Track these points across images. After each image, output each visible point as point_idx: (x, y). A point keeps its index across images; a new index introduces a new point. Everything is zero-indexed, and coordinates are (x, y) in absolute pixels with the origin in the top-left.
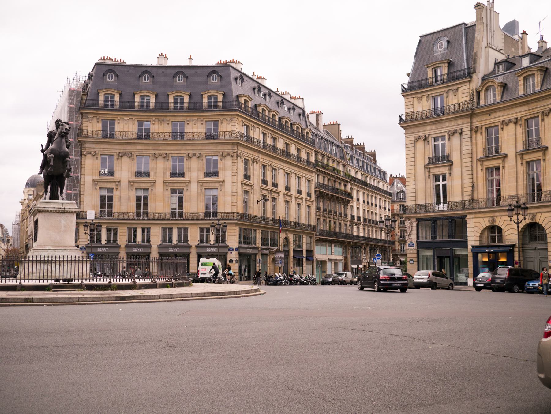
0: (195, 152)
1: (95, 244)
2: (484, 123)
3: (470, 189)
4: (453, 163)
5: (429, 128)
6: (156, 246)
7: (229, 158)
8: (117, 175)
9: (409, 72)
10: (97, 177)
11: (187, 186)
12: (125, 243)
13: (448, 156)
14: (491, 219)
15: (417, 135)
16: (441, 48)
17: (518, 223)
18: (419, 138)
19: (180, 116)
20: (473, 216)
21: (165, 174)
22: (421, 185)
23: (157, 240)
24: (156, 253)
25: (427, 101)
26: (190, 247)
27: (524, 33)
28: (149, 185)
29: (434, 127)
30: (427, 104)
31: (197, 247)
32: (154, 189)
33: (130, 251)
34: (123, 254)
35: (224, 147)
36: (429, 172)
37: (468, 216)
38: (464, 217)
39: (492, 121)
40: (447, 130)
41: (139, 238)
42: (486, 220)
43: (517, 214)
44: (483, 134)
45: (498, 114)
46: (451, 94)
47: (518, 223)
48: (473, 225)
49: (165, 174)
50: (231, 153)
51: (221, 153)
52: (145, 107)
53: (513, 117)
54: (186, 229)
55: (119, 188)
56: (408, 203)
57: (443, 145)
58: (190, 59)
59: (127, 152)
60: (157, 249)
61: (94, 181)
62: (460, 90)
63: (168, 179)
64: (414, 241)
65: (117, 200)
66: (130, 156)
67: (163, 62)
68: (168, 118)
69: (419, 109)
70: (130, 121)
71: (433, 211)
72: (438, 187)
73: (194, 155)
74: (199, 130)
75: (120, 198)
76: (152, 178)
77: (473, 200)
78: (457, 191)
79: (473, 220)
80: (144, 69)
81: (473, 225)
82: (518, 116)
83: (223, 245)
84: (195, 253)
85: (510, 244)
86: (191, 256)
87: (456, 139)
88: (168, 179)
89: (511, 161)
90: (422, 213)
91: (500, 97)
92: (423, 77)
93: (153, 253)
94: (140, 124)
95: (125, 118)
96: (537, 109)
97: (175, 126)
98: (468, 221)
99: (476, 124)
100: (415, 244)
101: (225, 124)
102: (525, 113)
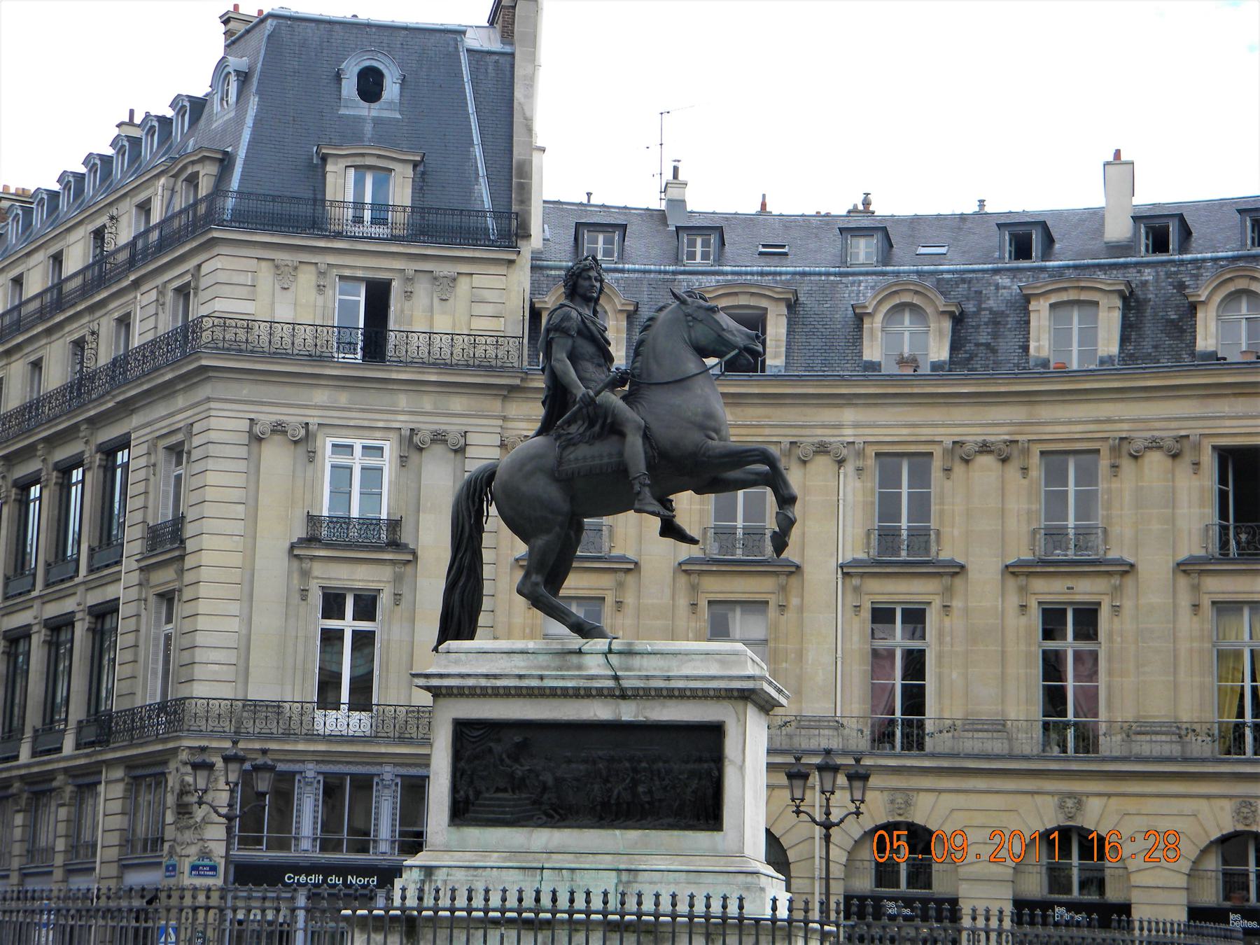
4: (414, 553)
5: (321, 396)
15: (267, 417)
17: (827, 826)
18: (279, 429)
22: (267, 621)
25: (320, 288)
29: (343, 398)
36: (305, 574)
47: (827, 826)
53: (998, 436)
56: (199, 690)
62: (463, 284)
69: (284, 313)
72: (331, 639)
89: (984, 586)
90: (270, 737)
96: (767, 431)
102: (905, 431)
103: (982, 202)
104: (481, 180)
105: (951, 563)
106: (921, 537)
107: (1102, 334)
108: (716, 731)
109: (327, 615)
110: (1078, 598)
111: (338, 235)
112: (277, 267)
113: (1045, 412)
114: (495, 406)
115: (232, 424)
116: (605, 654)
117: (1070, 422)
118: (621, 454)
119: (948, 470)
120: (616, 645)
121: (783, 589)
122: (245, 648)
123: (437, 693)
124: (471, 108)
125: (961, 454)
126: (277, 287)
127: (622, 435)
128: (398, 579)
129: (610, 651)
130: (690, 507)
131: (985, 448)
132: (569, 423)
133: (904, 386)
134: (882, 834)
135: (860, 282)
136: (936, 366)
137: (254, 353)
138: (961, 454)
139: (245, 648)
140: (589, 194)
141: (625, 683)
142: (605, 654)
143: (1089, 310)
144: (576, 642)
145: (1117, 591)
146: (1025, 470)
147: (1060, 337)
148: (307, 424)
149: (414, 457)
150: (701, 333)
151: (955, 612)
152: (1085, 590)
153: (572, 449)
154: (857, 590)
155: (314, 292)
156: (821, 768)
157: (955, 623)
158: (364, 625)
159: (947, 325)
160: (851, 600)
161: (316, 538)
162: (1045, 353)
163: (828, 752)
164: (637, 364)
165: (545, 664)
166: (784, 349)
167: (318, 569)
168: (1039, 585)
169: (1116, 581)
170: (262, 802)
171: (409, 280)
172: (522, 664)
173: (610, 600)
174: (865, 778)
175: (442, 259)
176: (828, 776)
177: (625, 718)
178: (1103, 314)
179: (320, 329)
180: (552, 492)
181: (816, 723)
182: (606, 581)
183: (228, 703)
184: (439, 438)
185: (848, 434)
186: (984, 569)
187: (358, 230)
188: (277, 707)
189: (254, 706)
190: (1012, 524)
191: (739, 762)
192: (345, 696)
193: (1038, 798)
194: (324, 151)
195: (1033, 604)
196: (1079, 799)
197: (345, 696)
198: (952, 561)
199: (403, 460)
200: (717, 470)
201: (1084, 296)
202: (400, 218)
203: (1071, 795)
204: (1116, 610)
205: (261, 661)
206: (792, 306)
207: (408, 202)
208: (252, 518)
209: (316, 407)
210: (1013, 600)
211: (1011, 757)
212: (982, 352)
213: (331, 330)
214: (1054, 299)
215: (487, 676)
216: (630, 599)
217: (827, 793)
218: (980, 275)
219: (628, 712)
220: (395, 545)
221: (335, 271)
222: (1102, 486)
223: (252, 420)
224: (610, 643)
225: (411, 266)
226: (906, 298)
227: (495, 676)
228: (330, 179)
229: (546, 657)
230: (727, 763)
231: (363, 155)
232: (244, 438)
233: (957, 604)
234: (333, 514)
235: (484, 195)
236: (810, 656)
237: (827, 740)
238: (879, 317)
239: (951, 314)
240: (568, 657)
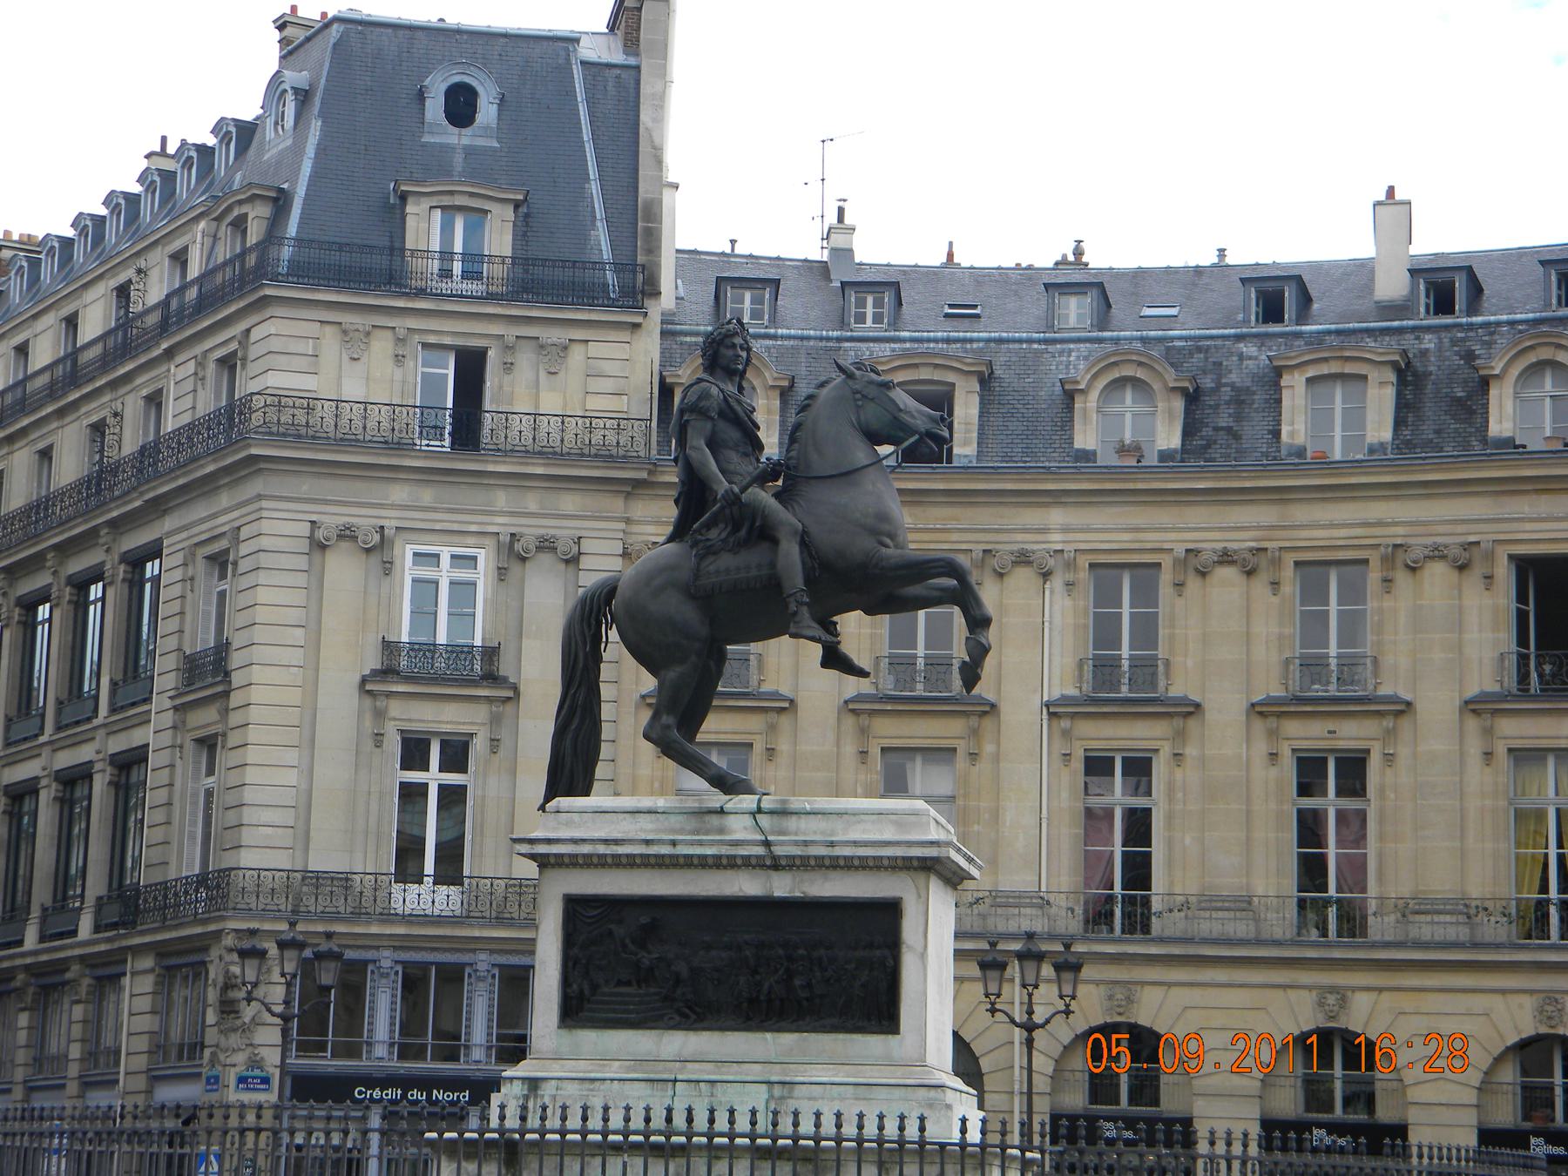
4: (515, 688)
5: (399, 493)
9: (963, 259)
15: (332, 519)
17: (1030, 1027)
22: (333, 772)
25: (399, 359)
29: (427, 495)
36: (380, 715)
42: (1306, 1000)
46: (525, 360)
47: (1030, 1027)
53: (1242, 542)
56: (248, 859)
62: (577, 355)
69: (353, 389)
72: (412, 795)
82: (1484, 535)
90: (336, 917)
96: (955, 537)
103: (1222, 252)
104: (599, 224)
105: (1183, 701)
106: (1146, 668)
107: (1371, 416)
108: (891, 910)
110: (1341, 744)
111: (421, 293)
112: (345, 332)
113: (1301, 513)
114: (616, 505)
116: (753, 814)
117: (1332, 526)
118: (773, 565)
119: (1179, 586)
120: (767, 803)
121: (975, 733)
122: (305, 807)
123: (544, 862)
124: (586, 134)
125: (1196, 565)
126: (345, 357)
127: (775, 542)
128: (495, 721)
129: (759, 810)
130: (859, 631)
131: (1226, 558)
132: (708, 526)
133: (1126, 480)
134: (1097, 1039)
135: (1070, 351)
136: (1165, 456)
137: (315, 439)
138: (1196, 565)
139: (305, 807)
140: (733, 242)
141: (778, 851)
142: (753, 814)
144: (717, 799)
147: (1320, 420)
148: (382, 527)
149: (516, 568)
150: (873, 415)
152: (1350, 734)
153: (711, 558)
154: (1066, 734)
155: (390, 363)
156: (1022, 956)
157: (1189, 775)
158: (453, 778)
159: (1179, 404)
160: (1060, 747)
161: (394, 670)
162: (1300, 440)
164: (793, 453)
165: (678, 826)
166: (975, 435)
167: (396, 708)
168: (1293, 728)
169: (1388, 722)
171: (509, 349)
172: (650, 826)
173: (758, 747)
174: (1076, 968)
176: (1030, 966)
177: (778, 893)
179: (398, 409)
180: (687, 613)
181: (1016, 900)
182: (755, 723)
183: (284, 874)
184: (546, 545)
185: (1056, 540)
187: (445, 287)
189: (317, 879)
191: (920, 949)
193: (1291, 993)
194: (403, 188)
195: (1286, 751)
196: (1343, 995)
197: (429, 866)
198: (1185, 698)
199: (502, 573)
200: (892, 585)
201: (1349, 369)
202: (498, 271)
203: (1333, 989)
204: (1389, 758)
206: (986, 381)
207: (507, 251)
208: (314, 645)
209: (393, 506)
210: (1261, 747)
211: (1259, 942)
212: (1222, 437)
213: (411, 411)
215: (606, 841)
216: (784, 746)
217: (1029, 986)
218: (1219, 342)
220: (491, 678)
221: (417, 338)
222: (1371, 604)
223: (313, 522)
224: (759, 801)
226: (1128, 371)
227: (616, 842)
228: (410, 222)
229: (680, 818)
230: (904, 949)
231: (451, 193)
232: (304, 546)
233: (1191, 751)
234: (414, 639)
235: (602, 243)
236: (1008, 817)
238: (1094, 395)
239: (1184, 391)
240: (707, 818)
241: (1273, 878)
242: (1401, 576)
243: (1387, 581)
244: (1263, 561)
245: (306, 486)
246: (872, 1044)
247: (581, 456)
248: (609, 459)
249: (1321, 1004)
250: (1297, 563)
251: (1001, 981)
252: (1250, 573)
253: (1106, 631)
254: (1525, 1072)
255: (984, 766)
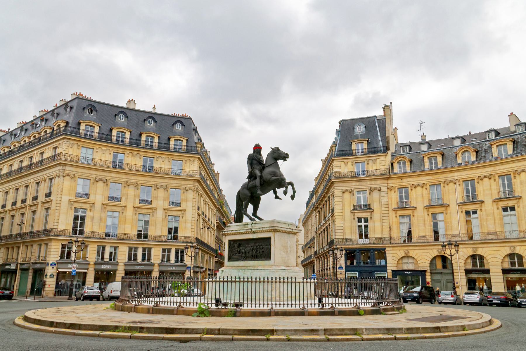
0: (162, 184)
1: (179, 263)
2: (397, 185)
3: (388, 229)
5: (354, 184)
6: (123, 264)
7: (190, 191)
8: (92, 198)
10: (73, 198)
11: (153, 212)
12: (94, 260)
13: (369, 205)
14: (406, 252)
15: (345, 188)
16: (360, 130)
18: (347, 190)
19: (151, 153)
20: (391, 248)
21: (134, 200)
22: (348, 224)
23: (124, 258)
24: (123, 269)
25: (352, 165)
26: (153, 265)
27: (396, 129)
28: (120, 208)
29: (358, 184)
30: (352, 167)
31: (159, 265)
32: (124, 212)
33: (98, 267)
34: (155, 274)
35: (187, 182)
36: (354, 215)
37: (387, 249)
38: (384, 249)
39: (404, 184)
40: (369, 186)
41: (107, 256)
43: (451, 249)
44: (396, 192)
45: (409, 179)
48: (391, 255)
49: (134, 200)
50: (193, 188)
51: (184, 187)
52: (120, 142)
53: (487, 174)
54: (150, 250)
55: (93, 209)
56: (337, 237)
57: (364, 197)
58: (154, 108)
59: (103, 178)
60: (123, 267)
61: (70, 201)
62: (378, 160)
63: (137, 204)
64: (343, 265)
65: (90, 220)
66: (105, 182)
67: (132, 106)
68: (141, 153)
69: (346, 170)
70: (108, 151)
71: (358, 244)
72: (360, 226)
73: (162, 186)
74: (166, 167)
75: (92, 219)
76: (123, 203)
77: (390, 238)
78: (377, 231)
79: (391, 252)
80: (120, 110)
81: (391, 255)
82: (425, 182)
83: (182, 264)
84: (157, 270)
85: (422, 269)
86: (117, 272)
87: (376, 194)
88: (137, 204)
90: (350, 245)
91: (409, 168)
92: (347, 148)
93: (119, 269)
94: (115, 156)
95: (103, 148)
97: (145, 161)
98: (387, 252)
99: (390, 185)
100: (344, 268)
101: (188, 163)
105: (481, 201)
106: (474, 196)
107: (508, 150)
108: (269, 238)
109: (359, 222)
110: (510, 205)
111: (355, 155)
113: (498, 168)
114: (385, 181)
115: (339, 191)
119: (478, 182)
121: (446, 210)
122: (344, 229)
124: (378, 129)
125: (481, 179)
128: (371, 215)
131: (485, 177)
133: (467, 166)
134: (473, 257)
136: (473, 162)
137: (341, 178)
138: (481, 179)
139: (344, 229)
143: (505, 146)
145: (518, 202)
146: (495, 180)
147: (499, 152)
149: (372, 192)
150: (276, 155)
151: (483, 211)
152: (511, 203)
154: (461, 208)
156: (448, 244)
157: (483, 213)
158: (366, 224)
159: (475, 153)
160: (460, 210)
161: (356, 208)
162: (496, 156)
163: (450, 241)
167: (356, 214)
168: (501, 203)
169: (518, 200)
170: (351, 255)
173: (412, 215)
174: (458, 246)
175: (373, 156)
176: (450, 246)
178: (508, 146)
181: (455, 235)
182: (411, 211)
184: (376, 189)
185: (456, 178)
186: (488, 202)
188: (351, 239)
189: (346, 239)
190: (493, 191)
192: (364, 237)
193: (505, 248)
195: (500, 207)
196: (514, 247)
197: (364, 237)
199: (370, 193)
201: (503, 143)
203: (512, 246)
204: (518, 206)
205: (348, 231)
206: (443, 155)
207: (367, 147)
210: (495, 207)
211: (498, 239)
212: (483, 157)
214: (497, 144)
216: (415, 214)
217: (451, 249)
219: (255, 236)
220: (370, 209)
222: (513, 181)
225: (368, 159)
226: (465, 149)
233: (483, 209)
235: (381, 144)
236: (453, 222)
237: (457, 239)
238: (460, 154)
239: (475, 151)
241: (430, 234)
242: (517, 176)
243: (412, 190)
244: (492, 176)
245: (341, 184)
246: (266, 262)
247: (381, 175)
248: (383, 175)
249: (438, 251)
250: (499, 176)
251: (458, 248)
252: (490, 179)
253: (401, 198)
254: (510, 259)
255: (448, 214)
